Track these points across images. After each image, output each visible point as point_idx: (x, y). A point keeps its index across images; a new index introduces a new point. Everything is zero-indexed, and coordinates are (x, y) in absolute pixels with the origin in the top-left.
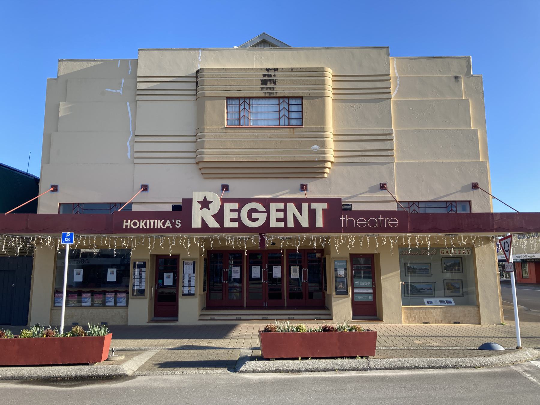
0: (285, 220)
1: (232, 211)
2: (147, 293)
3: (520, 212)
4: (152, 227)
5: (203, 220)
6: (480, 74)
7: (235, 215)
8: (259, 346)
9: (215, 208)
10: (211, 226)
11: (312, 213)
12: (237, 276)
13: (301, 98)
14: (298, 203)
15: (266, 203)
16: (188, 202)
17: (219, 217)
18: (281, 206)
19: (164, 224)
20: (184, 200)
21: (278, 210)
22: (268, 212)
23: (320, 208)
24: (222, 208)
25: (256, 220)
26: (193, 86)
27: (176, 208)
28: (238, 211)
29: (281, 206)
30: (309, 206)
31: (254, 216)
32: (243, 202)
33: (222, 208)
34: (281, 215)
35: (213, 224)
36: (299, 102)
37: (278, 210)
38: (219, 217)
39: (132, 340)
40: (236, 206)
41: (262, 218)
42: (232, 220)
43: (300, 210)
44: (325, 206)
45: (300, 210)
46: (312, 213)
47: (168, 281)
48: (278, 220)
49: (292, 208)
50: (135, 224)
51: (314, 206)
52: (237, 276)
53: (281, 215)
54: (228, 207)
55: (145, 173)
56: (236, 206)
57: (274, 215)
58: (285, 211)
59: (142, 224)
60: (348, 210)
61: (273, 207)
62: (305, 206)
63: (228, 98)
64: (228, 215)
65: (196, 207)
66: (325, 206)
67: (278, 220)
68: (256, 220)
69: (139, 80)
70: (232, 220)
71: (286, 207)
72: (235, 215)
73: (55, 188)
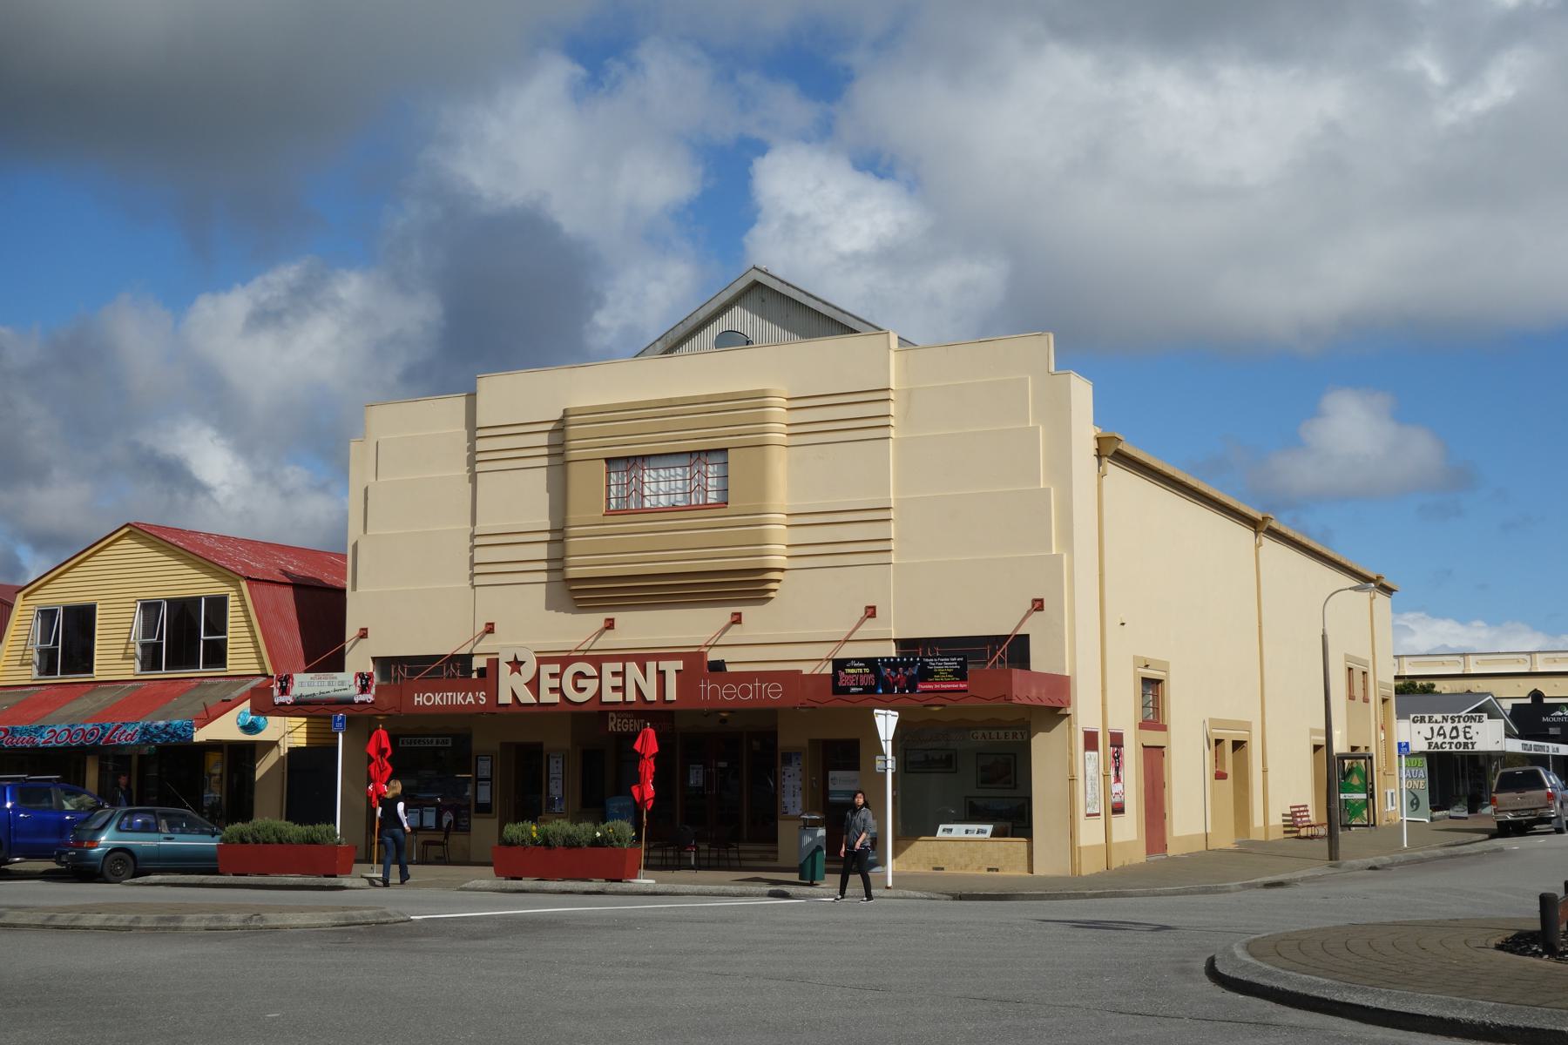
7: (555, 683)
9: (528, 671)
11: (661, 674)
12: (486, 774)
13: (726, 450)
16: (494, 663)
18: (618, 667)
19: (464, 699)
21: (615, 674)
22: (600, 677)
23: (672, 668)
25: (584, 689)
29: (618, 667)
30: (538, 697)
31: (581, 683)
34: (618, 681)
35: (527, 697)
36: (719, 458)
37: (615, 674)
38: (534, 685)
39: (1308, 1013)
40: (556, 668)
41: (591, 686)
42: (552, 690)
44: (680, 665)
46: (661, 674)
47: (1552, 731)
48: (615, 689)
49: (633, 669)
50: (429, 699)
51: (663, 665)
52: (486, 774)
53: (618, 681)
55: (493, 603)
56: (556, 668)
57: (609, 681)
58: (623, 674)
60: (718, 666)
61: (608, 668)
63: (608, 460)
64: (546, 683)
65: (504, 670)
66: (680, 665)
67: (615, 689)
68: (584, 689)
69: (479, 433)
70: (552, 690)
72: (555, 683)
73: (364, 634)
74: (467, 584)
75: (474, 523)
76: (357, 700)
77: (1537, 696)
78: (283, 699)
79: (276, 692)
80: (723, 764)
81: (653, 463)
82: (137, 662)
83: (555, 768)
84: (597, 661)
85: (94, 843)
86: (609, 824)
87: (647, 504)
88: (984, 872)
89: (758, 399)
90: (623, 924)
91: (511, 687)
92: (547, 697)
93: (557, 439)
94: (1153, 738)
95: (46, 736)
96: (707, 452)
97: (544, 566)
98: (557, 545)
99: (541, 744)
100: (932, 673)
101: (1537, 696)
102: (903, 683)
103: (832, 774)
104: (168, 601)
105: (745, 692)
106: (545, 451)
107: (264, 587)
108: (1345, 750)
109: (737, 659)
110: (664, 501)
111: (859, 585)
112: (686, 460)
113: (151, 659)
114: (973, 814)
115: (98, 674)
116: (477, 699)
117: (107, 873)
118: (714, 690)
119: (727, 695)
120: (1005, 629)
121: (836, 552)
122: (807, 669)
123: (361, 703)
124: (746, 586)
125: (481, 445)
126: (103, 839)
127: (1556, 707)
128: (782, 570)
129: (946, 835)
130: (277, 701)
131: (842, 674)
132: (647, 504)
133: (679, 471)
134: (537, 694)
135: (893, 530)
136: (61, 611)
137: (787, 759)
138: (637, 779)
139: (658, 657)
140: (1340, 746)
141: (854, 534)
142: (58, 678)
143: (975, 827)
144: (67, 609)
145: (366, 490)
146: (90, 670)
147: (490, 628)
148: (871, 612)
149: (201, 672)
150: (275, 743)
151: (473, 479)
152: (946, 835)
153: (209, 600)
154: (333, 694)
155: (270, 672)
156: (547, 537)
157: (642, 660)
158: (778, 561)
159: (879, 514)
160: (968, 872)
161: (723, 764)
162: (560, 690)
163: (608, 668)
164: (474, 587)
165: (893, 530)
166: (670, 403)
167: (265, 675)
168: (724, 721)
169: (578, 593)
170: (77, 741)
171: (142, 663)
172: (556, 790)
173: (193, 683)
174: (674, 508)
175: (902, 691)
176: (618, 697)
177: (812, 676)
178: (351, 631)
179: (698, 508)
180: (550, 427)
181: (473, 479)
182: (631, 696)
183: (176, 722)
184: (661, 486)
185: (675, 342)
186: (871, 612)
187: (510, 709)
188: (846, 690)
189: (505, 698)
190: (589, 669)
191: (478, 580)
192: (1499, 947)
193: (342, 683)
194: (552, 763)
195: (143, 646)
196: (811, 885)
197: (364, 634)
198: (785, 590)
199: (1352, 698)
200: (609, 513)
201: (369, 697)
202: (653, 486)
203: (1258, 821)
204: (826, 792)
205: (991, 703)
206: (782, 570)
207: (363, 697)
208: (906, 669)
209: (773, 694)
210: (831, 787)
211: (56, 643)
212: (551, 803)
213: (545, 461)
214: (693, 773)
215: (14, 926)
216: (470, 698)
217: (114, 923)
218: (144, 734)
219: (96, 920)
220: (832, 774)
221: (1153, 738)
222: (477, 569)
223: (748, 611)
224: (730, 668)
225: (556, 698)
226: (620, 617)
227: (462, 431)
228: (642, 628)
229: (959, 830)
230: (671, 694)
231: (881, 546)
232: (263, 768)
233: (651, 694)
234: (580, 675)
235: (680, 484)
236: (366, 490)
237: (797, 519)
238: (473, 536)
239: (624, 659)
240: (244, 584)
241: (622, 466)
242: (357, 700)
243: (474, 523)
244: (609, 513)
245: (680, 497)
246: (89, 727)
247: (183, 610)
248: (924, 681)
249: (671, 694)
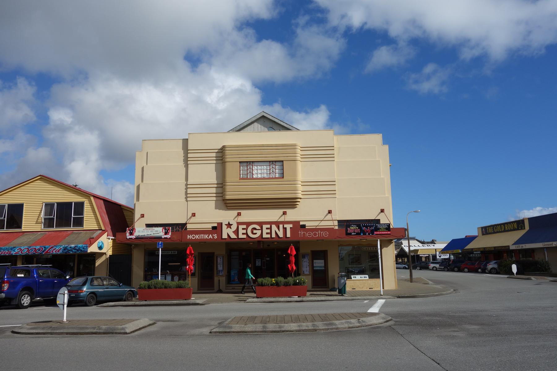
0: (271, 233)
1: (243, 229)
2: (197, 274)
5: (228, 235)
7: (245, 231)
9: (234, 227)
10: (232, 237)
11: (285, 229)
13: (283, 161)
14: (277, 224)
15: (261, 224)
17: (236, 232)
18: (269, 226)
19: (208, 237)
20: (218, 223)
21: (267, 229)
22: (262, 229)
23: (288, 227)
24: (238, 228)
25: (256, 234)
27: (214, 228)
28: (246, 229)
29: (269, 226)
31: (255, 231)
32: (248, 224)
33: (238, 228)
34: (269, 231)
35: (233, 236)
37: (267, 229)
38: (236, 232)
40: (245, 227)
41: (259, 233)
42: (243, 234)
44: (291, 226)
46: (285, 229)
48: (267, 233)
49: (274, 227)
50: (193, 237)
51: (285, 226)
53: (269, 231)
54: (241, 227)
55: (194, 207)
56: (245, 227)
57: (265, 231)
58: (271, 228)
59: (197, 237)
60: (304, 226)
61: (265, 227)
62: (281, 226)
63: (240, 162)
64: (241, 231)
65: (224, 227)
66: (291, 226)
67: (267, 233)
68: (256, 234)
70: (243, 234)
71: (271, 227)
72: (245, 231)
74: (184, 200)
75: (187, 179)
76: (163, 237)
78: (131, 237)
79: (128, 234)
80: (268, 259)
81: (256, 164)
82: (43, 225)
83: (220, 260)
85: (82, 291)
86: (300, 277)
87: (254, 177)
88: (368, 289)
89: (293, 146)
91: (226, 233)
92: (241, 236)
93: (220, 155)
95: (16, 251)
96: (275, 161)
97: (215, 195)
98: (220, 189)
99: (214, 253)
100: (379, 229)
102: (369, 232)
103: (315, 261)
104: (57, 203)
105: (315, 234)
106: (215, 159)
110: (259, 176)
111: (328, 203)
112: (268, 164)
113: (49, 223)
114: (361, 272)
115: (24, 229)
116: (213, 237)
117: (88, 303)
118: (304, 234)
120: (373, 218)
121: (318, 193)
123: (165, 238)
124: (290, 203)
126: (85, 289)
128: (301, 198)
129: (354, 279)
130: (128, 237)
131: (349, 229)
132: (254, 177)
133: (265, 167)
134: (238, 235)
135: (336, 188)
136: (7, 206)
137: (304, 256)
138: (289, 262)
141: (325, 189)
142: (55, 229)
143: (363, 276)
144: (10, 206)
145: (143, 168)
146: (20, 227)
147: (194, 215)
148: (330, 212)
149: (72, 228)
150: (105, 253)
151: (187, 166)
152: (354, 279)
153: (76, 203)
154: (153, 235)
155: (103, 229)
156: (216, 186)
158: (300, 196)
159: (332, 183)
160: (364, 289)
161: (268, 259)
162: (247, 234)
164: (187, 201)
165: (336, 188)
166: (263, 146)
167: (101, 230)
169: (226, 203)
170: (31, 252)
171: (44, 225)
172: (220, 268)
173: (69, 232)
174: (264, 178)
175: (369, 234)
176: (269, 236)
178: (137, 215)
179: (272, 178)
180: (216, 151)
181: (187, 166)
182: (274, 235)
183: (80, 245)
184: (259, 171)
185: (240, 129)
186: (330, 212)
187: (227, 240)
188: (350, 234)
189: (225, 236)
190: (258, 227)
191: (188, 199)
193: (157, 231)
194: (219, 259)
195: (45, 219)
196: (342, 295)
197: (143, 216)
198: (301, 204)
200: (240, 179)
201: (168, 236)
202: (256, 171)
204: (313, 266)
205: (343, 239)
206: (301, 198)
207: (166, 236)
208: (370, 227)
210: (314, 265)
211: (5, 217)
212: (218, 272)
213: (215, 162)
214: (257, 262)
215: (245, 332)
216: (211, 236)
217: (304, 328)
218: (65, 250)
219: (293, 326)
222: (188, 195)
223: (289, 211)
225: (245, 236)
226: (243, 212)
227: (181, 152)
228: (249, 215)
229: (358, 277)
230: (289, 235)
231: (333, 193)
232: (98, 263)
233: (281, 234)
234: (255, 229)
235: (265, 171)
236: (143, 168)
237: (305, 183)
238: (187, 185)
239: (271, 223)
240: (92, 198)
241: (245, 164)
242: (163, 237)
243: (187, 179)
244: (240, 179)
245: (265, 175)
246: (38, 247)
247: (64, 207)
248: (377, 231)
249: (289, 235)
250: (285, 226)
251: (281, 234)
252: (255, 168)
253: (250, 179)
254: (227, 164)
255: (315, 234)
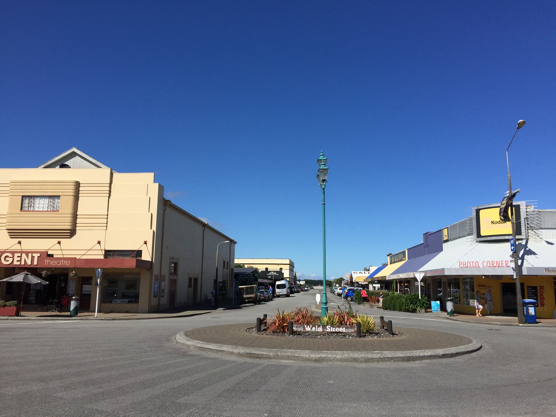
0: (20, 261)
3: (535, 266)
4: (525, 313)
6: (222, 262)
8: (511, 233)
11: (33, 258)
18: (19, 255)
22: (13, 257)
23: (36, 256)
26: (106, 217)
31: (7, 259)
34: (19, 259)
41: (11, 260)
43: (28, 257)
45: (28, 257)
46: (33, 258)
48: (18, 261)
49: (24, 256)
51: (34, 255)
53: (19, 259)
57: (16, 259)
58: (21, 256)
61: (16, 255)
62: (30, 255)
66: (39, 255)
77: (267, 269)
84: (13, 253)
90: (21, 329)
94: (173, 277)
101: (267, 269)
103: (84, 286)
105: (59, 263)
107: (201, 261)
108: (221, 281)
109: (57, 254)
118: (49, 262)
119: (53, 264)
121: (91, 226)
122: (78, 257)
125: (106, 217)
127: (270, 271)
132: (40, 210)
139: (32, 253)
140: (220, 279)
148: (99, 243)
157: (27, 253)
163: (16, 255)
168: (53, 271)
169: (14, 233)
176: (19, 263)
177: (79, 259)
182: (23, 263)
190: (10, 255)
192: (535, 254)
199: (224, 267)
203: (199, 298)
209: (67, 264)
210: (83, 289)
220: (84, 286)
221: (173, 277)
224: (55, 256)
228: (29, 244)
230: (35, 263)
233: (29, 262)
239: (22, 252)
249: (35, 263)
250: (34, 255)
251: (29, 262)
252: (286, 293)
253: (31, 211)
254: (72, 194)
255: (59, 263)
